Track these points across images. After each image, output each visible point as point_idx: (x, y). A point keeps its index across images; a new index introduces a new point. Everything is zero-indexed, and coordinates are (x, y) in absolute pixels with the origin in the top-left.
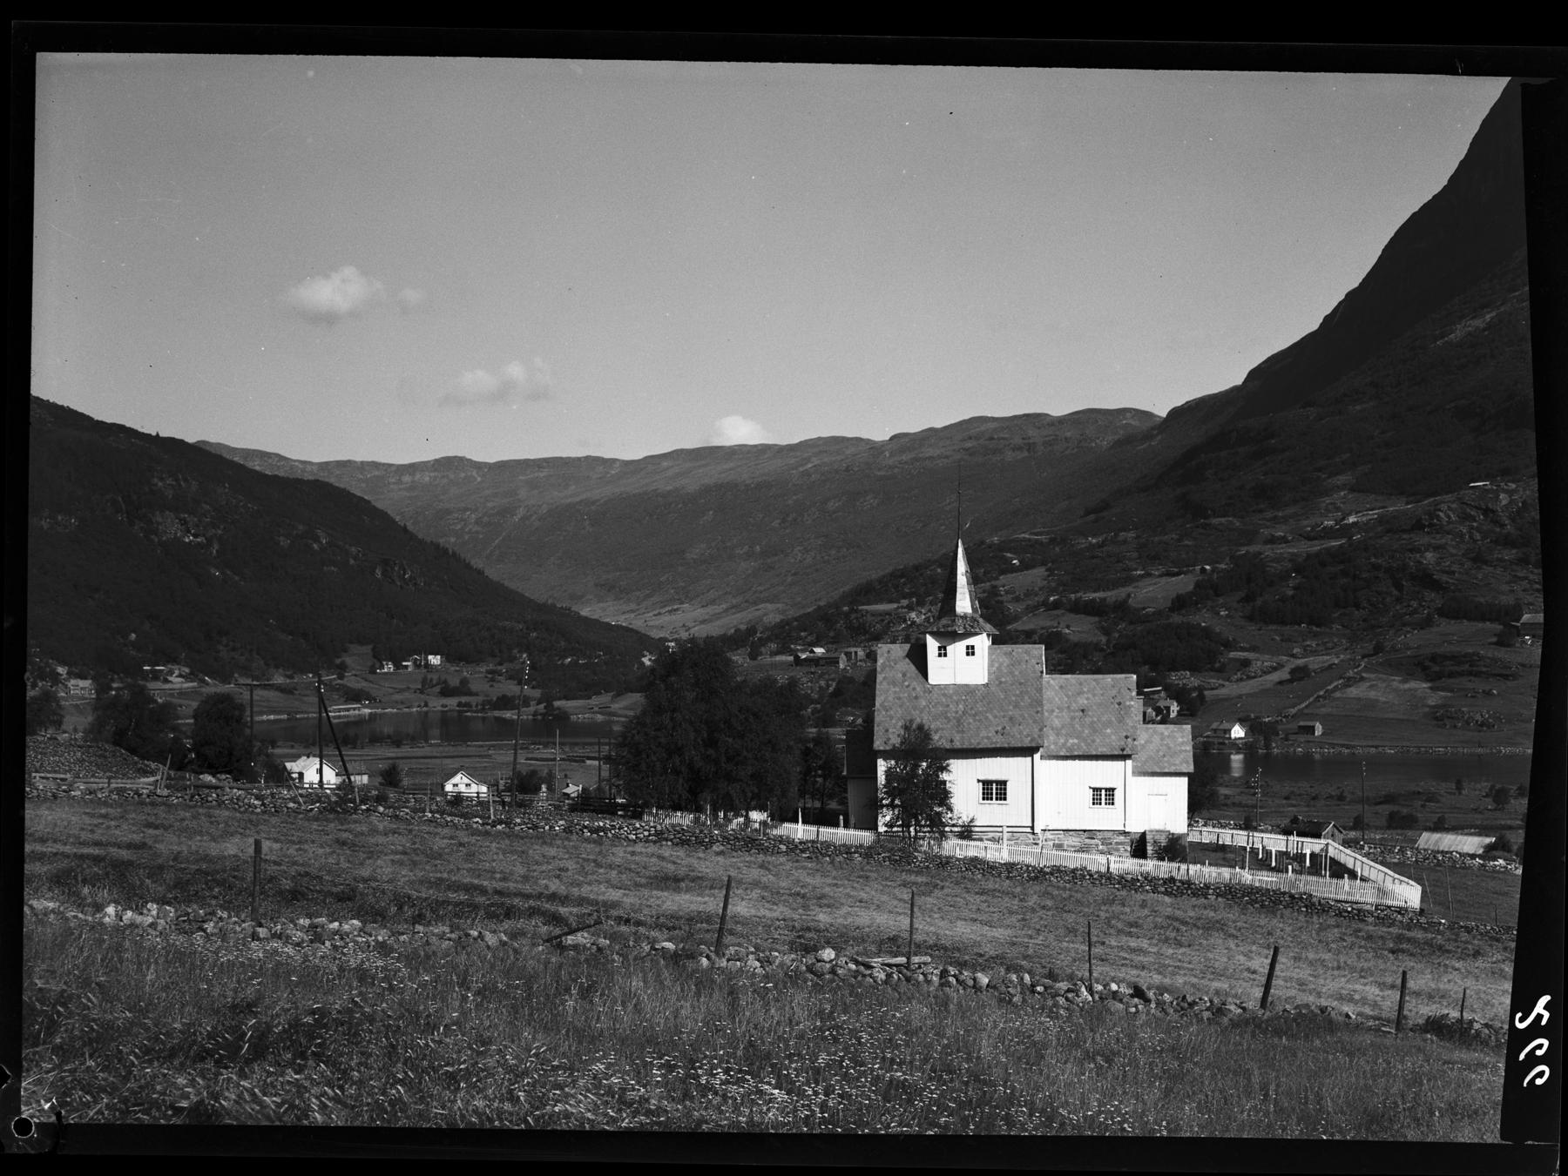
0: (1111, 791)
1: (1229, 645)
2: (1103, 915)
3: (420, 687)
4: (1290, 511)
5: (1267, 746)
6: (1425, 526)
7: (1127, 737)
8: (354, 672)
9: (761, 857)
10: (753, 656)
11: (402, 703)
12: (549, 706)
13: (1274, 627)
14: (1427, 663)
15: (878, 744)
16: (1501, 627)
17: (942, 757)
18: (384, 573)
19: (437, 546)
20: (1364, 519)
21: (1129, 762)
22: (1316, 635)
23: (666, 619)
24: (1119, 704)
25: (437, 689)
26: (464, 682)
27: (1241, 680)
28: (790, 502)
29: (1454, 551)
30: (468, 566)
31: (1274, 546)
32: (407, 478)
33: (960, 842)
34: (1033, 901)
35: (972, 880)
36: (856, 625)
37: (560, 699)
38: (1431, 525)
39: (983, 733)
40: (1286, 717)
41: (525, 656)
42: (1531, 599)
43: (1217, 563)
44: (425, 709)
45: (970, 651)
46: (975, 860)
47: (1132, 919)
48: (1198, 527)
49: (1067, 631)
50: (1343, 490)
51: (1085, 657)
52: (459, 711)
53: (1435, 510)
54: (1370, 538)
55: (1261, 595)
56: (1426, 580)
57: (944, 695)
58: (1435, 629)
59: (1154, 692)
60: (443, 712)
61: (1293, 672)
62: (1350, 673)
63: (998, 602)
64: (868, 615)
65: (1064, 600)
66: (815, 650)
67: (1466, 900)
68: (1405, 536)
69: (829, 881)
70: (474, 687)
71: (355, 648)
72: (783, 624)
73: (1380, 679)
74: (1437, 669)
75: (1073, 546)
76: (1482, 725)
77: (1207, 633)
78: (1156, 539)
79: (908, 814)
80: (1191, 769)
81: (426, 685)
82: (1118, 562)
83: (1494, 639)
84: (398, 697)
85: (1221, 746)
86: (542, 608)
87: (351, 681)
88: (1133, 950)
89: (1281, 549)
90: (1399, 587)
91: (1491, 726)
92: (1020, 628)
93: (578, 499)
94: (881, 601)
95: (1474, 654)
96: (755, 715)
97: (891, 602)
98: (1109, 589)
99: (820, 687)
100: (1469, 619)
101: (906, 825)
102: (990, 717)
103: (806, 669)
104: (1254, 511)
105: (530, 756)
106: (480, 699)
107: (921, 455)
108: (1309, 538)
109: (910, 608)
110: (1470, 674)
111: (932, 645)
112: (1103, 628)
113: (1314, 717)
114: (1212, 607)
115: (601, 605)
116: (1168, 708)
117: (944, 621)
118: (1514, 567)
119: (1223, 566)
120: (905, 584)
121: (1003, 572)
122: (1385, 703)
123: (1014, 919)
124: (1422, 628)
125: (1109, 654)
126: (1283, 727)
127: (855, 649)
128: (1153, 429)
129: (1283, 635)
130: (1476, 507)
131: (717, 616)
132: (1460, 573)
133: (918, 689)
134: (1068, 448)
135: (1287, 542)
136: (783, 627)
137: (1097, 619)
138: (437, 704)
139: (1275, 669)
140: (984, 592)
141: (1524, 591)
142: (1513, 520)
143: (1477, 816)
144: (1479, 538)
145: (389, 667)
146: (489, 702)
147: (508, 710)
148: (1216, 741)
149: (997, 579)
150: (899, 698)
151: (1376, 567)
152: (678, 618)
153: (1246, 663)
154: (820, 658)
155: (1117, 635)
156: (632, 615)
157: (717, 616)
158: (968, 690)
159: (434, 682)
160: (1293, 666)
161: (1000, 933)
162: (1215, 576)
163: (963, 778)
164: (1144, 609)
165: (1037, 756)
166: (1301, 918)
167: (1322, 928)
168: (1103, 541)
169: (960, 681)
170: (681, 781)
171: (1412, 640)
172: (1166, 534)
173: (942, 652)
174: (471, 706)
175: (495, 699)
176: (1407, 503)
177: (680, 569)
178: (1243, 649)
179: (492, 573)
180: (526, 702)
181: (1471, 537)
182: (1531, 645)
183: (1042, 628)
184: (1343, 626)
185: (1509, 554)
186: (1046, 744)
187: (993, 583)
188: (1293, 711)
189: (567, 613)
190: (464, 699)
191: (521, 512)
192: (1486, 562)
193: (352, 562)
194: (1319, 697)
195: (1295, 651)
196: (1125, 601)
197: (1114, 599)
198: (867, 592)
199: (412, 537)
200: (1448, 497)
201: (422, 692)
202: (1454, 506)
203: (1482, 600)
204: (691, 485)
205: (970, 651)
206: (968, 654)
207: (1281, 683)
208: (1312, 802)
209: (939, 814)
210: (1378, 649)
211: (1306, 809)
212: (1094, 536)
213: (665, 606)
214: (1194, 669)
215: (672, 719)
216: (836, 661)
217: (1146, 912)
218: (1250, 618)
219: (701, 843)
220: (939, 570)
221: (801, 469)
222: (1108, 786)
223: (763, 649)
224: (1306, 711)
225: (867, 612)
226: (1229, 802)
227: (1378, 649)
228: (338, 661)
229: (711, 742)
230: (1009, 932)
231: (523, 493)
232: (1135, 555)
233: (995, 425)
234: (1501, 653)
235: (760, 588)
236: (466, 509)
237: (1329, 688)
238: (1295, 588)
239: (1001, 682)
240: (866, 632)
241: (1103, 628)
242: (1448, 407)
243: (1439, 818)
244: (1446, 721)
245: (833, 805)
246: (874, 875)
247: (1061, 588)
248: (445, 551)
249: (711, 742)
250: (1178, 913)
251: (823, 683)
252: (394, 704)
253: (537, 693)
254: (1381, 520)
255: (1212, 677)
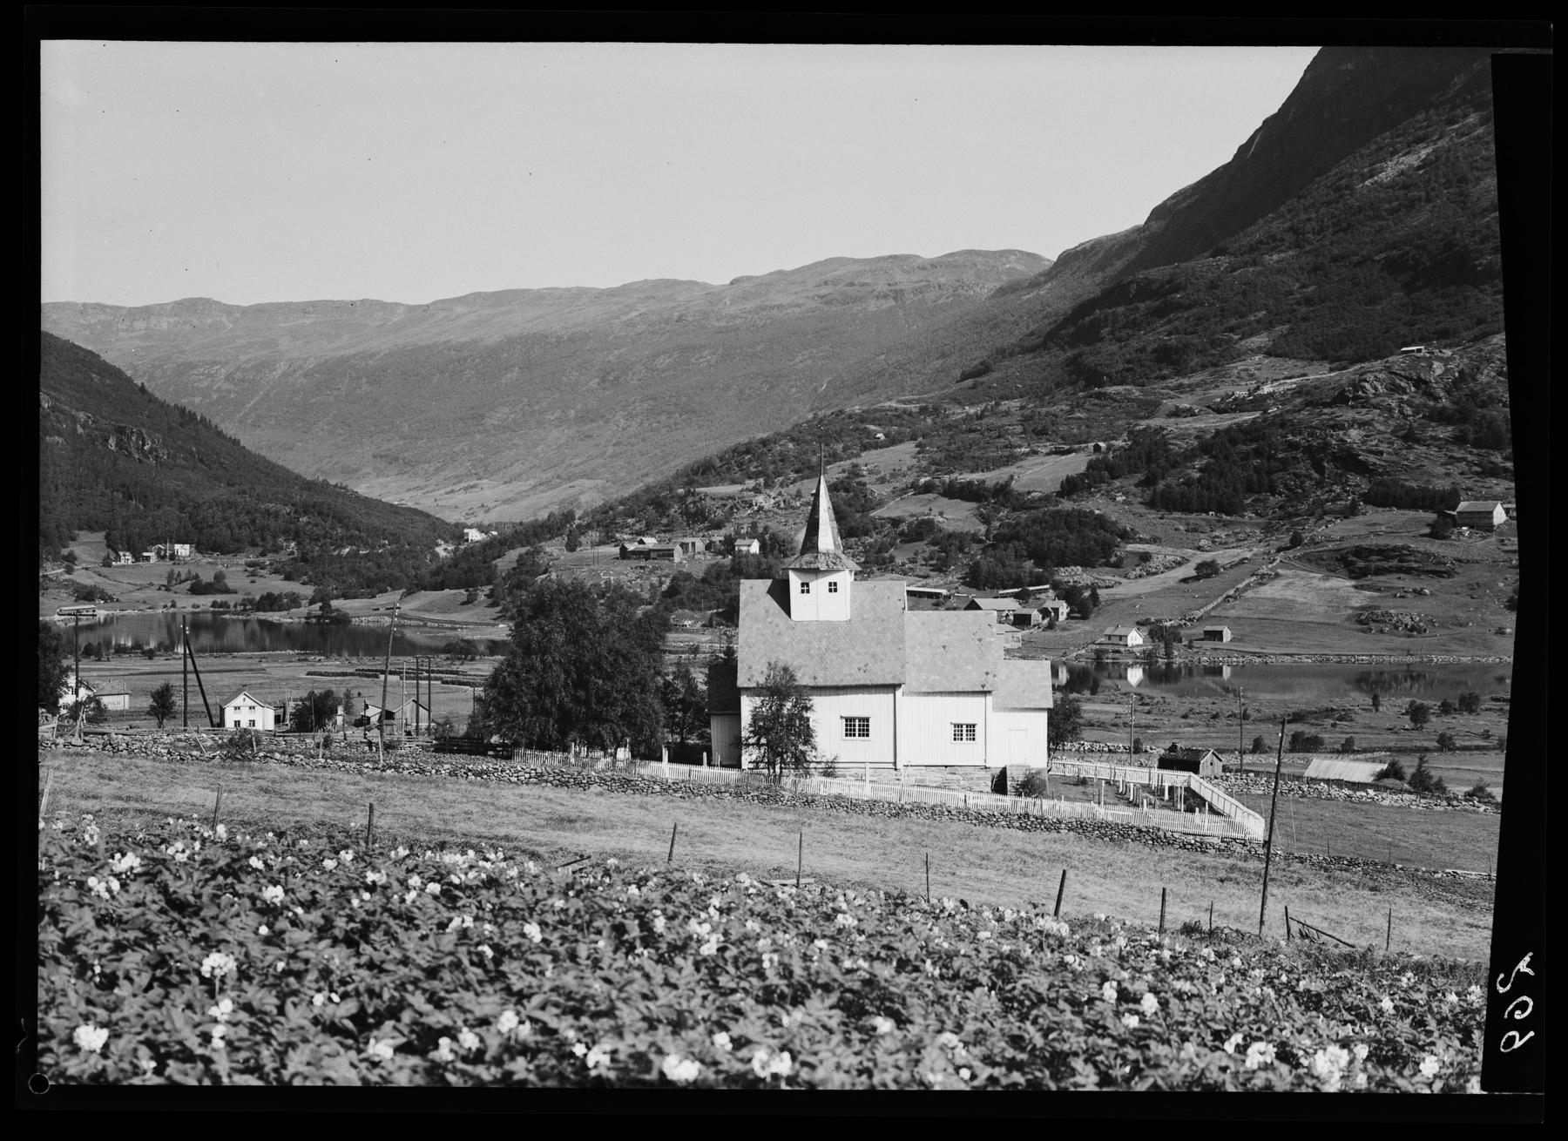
0: (971, 727)
1: (1126, 536)
2: (957, 849)
3: (166, 583)
4: (1197, 378)
5: (1168, 655)
6: (1348, 399)
7: (987, 674)
8: (84, 565)
9: (638, 798)
10: (571, 547)
11: (144, 602)
12: (326, 607)
13: (1177, 515)
14: (1351, 558)
15: (742, 682)
16: (1435, 516)
17: (803, 694)
18: (119, 444)
19: (182, 411)
20: (1281, 389)
21: (989, 698)
22: (1226, 525)
23: (460, 497)
24: (980, 640)
25: (188, 585)
26: (219, 577)
27: (1140, 576)
28: (611, 358)
29: (1382, 428)
30: (220, 434)
31: (1179, 420)
32: (140, 325)
33: (824, 779)
34: (894, 835)
35: (837, 817)
36: (693, 510)
37: (337, 598)
38: (1356, 398)
39: (846, 671)
40: (1190, 620)
41: (293, 545)
42: (1469, 483)
43: (1113, 439)
44: (172, 610)
45: (833, 587)
46: (838, 797)
47: (983, 853)
48: (1091, 396)
49: (941, 519)
50: (1258, 353)
51: (961, 550)
52: (213, 612)
53: (1360, 381)
54: (1288, 411)
55: (1163, 478)
56: (1349, 461)
57: (807, 631)
58: (1360, 518)
59: (1040, 591)
60: (193, 613)
61: (1199, 567)
62: (1264, 570)
63: (859, 483)
64: (708, 499)
65: (937, 482)
66: (645, 539)
67: (1317, 831)
68: (1325, 411)
69: (705, 819)
70: (230, 583)
71: (85, 536)
72: (606, 509)
73: (1296, 576)
74: (1361, 564)
75: (947, 416)
76: (1412, 629)
77: (1101, 522)
78: (1044, 410)
79: (774, 753)
80: (1051, 706)
81: (172, 581)
82: (999, 437)
83: (1427, 530)
84: (138, 595)
85: (1117, 655)
86: (310, 486)
87: (83, 577)
88: (979, 880)
89: (1187, 424)
90: (1321, 470)
91: (1421, 631)
92: (886, 515)
93: (352, 351)
94: (722, 481)
95: (1403, 548)
96: (625, 658)
97: (734, 482)
98: (988, 469)
99: (652, 585)
100: (1399, 507)
101: (771, 764)
102: (853, 654)
103: (635, 563)
104: (1156, 378)
105: (312, 669)
106: (239, 597)
107: (768, 303)
108: (1219, 411)
109: (757, 490)
110: (1399, 570)
111: (795, 581)
112: (981, 515)
113: (1221, 619)
114: (1108, 492)
115: (381, 480)
116: (1056, 610)
117: (807, 557)
118: (1450, 447)
119: (1119, 443)
120: (750, 461)
121: (865, 448)
122: (1302, 603)
123: (876, 853)
124: (1346, 518)
125: (990, 545)
126: (1188, 632)
127: (693, 540)
128: (1040, 275)
129: (1188, 524)
130: (1406, 377)
131: (523, 495)
132: (1389, 453)
133: (781, 625)
134: (942, 296)
135: (1193, 415)
136: (606, 512)
137: (973, 505)
138: (187, 604)
139: (1180, 564)
140: (844, 471)
141: (1461, 474)
142: (1448, 392)
143: (1392, 737)
144: (1410, 413)
145: (127, 558)
146: (251, 601)
147: (274, 611)
148: (1110, 648)
149: (858, 455)
150: (763, 635)
151: (1293, 446)
152: (474, 498)
153: (1145, 557)
154: (651, 550)
155: (998, 524)
156: (420, 493)
157: (523, 495)
158: (831, 627)
159: (183, 577)
160: (1199, 561)
161: (863, 865)
162: (1111, 456)
163: (826, 716)
164: (1029, 493)
165: (899, 692)
166: (1147, 850)
167: (1161, 859)
168: (983, 412)
169: (824, 617)
170: (551, 721)
171: (1339, 532)
172: (1055, 404)
173: (805, 587)
174: (228, 607)
175: (257, 598)
176: (1331, 370)
177: (478, 437)
178: (1142, 541)
179: (248, 441)
180: (294, 601)
181: (1401, 412)
182: (1470, 537)
183: (913, 516)
184: (1257, 514)
185: (1444, 432)
186: (908, 681)
187: (855, 460)
188: (1198, 614)
189: (342, 492)
190: (219, 598)
191: (282, 367)
192: (1418, 441)
193: (80, 430)
194: (1228, 597)
195: (1202, 543)
196: (1007, 484)
197: (994, 482)
198: (704, 471)
199: (151, 399)
200: (1378, 364)
201: (168, 590)
202: (1381, 376)
203: (1414, 485)
204: (492, 336)
205: (833, 587)
206: (830, 590)
207: (1185, 580)
208: (1212, 722)
209: (803, 753)
210: (1296, 541)
211: (1204, 730)
212: (972, 404)
213: (460, 482)
214: (1087, 563)
215: (542, 661)
216: (669, 554)
217: (998, 846)
218: (1151, 504)
219: (580, 784)
220: (791, 445)
221: (624, 318)
222: (969, 722)
223: (583, 539)
224: (1213, 614)
225: (706, 495)
226: (1119, 721)
227: (1296, 541)
228: (65, 552)
229: (581, 683)
230: (872, 865)
231: (284, 344)
232: (1019, 429)
233: (856, 268)
234: (1435, 547)
235: (576, 461)
236: (214, 363)
237: (1240, 586)
238: (1200, 470)
239: (863, 619)
240: (705, 519)
241: (981, 515)
242: (1377, 258)
243: (1347, 740)
244: (1373, 625)
245: (693, 741)
246: (745, 814)
247: (933, 468)
248: (192, 416)
249: (581, 683)
250: (1029, 848)
251: (654, 580)
252: (134, 604)
253: (309, 591)
254: (1299, 391)
255: (1107, 573)
